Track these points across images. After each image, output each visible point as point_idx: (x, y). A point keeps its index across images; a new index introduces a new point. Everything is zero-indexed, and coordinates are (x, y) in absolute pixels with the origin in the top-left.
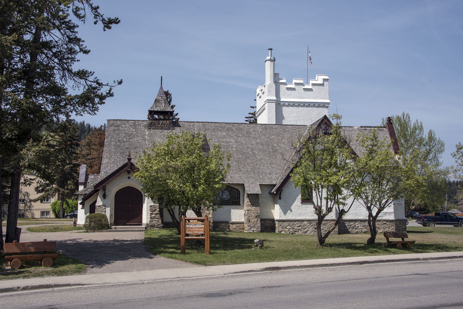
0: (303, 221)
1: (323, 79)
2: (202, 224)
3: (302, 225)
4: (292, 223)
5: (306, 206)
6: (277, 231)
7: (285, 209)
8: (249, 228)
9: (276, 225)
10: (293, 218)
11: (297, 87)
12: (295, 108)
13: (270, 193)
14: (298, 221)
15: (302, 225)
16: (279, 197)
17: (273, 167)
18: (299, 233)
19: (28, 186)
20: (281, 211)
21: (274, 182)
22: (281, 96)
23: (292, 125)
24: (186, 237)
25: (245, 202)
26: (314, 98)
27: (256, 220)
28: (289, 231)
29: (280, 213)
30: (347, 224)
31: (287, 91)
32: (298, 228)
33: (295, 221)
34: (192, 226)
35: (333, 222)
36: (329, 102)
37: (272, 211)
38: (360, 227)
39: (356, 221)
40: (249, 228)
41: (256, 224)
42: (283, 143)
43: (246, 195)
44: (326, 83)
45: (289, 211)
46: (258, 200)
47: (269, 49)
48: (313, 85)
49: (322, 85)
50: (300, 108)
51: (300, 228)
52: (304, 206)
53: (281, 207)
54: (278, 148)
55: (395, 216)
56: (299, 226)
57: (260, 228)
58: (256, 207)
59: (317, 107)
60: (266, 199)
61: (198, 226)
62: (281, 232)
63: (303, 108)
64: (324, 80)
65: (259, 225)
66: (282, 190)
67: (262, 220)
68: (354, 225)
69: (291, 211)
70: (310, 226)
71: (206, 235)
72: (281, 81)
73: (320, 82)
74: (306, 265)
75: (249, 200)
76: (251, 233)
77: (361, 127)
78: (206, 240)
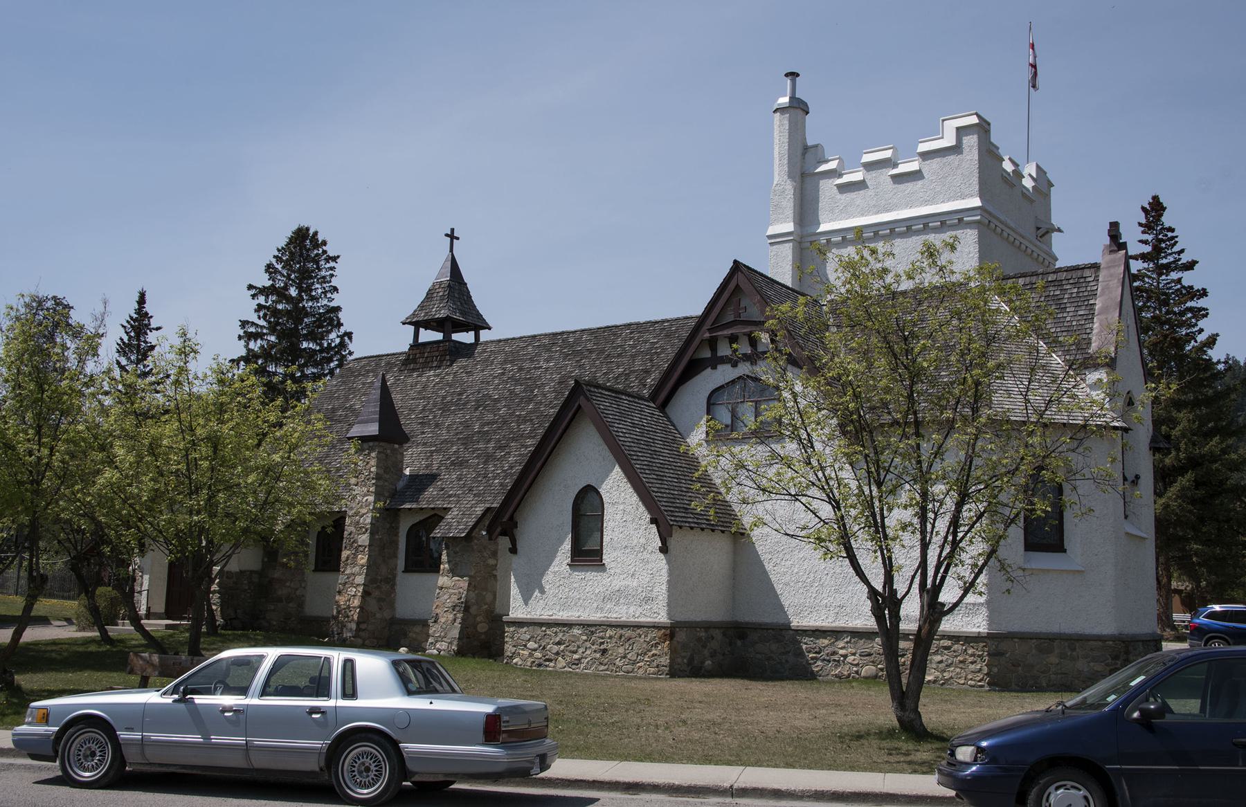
0: (568, 625)
1: (958, 129)
4: (539, 631)
5: (581, 575)
11: (871, 178)
18: (559, 665)
19: (821, 552)
22: (821, 218)
26: (926, 202)
28: (531, 655)
30: (806, 644)
31: (839, 196)
32: (555, 649)
38: (850, 659)
39: (836, 634)
45: (537, 593)
47: (787, 75)
52: (579, 575)
55: (991, 620)
56: (559, 643)
57: (455, 643)
64: (960, 131)
68: (830, 650)
69: (542, 591)
73: (949, 140)
74: (784, 788)
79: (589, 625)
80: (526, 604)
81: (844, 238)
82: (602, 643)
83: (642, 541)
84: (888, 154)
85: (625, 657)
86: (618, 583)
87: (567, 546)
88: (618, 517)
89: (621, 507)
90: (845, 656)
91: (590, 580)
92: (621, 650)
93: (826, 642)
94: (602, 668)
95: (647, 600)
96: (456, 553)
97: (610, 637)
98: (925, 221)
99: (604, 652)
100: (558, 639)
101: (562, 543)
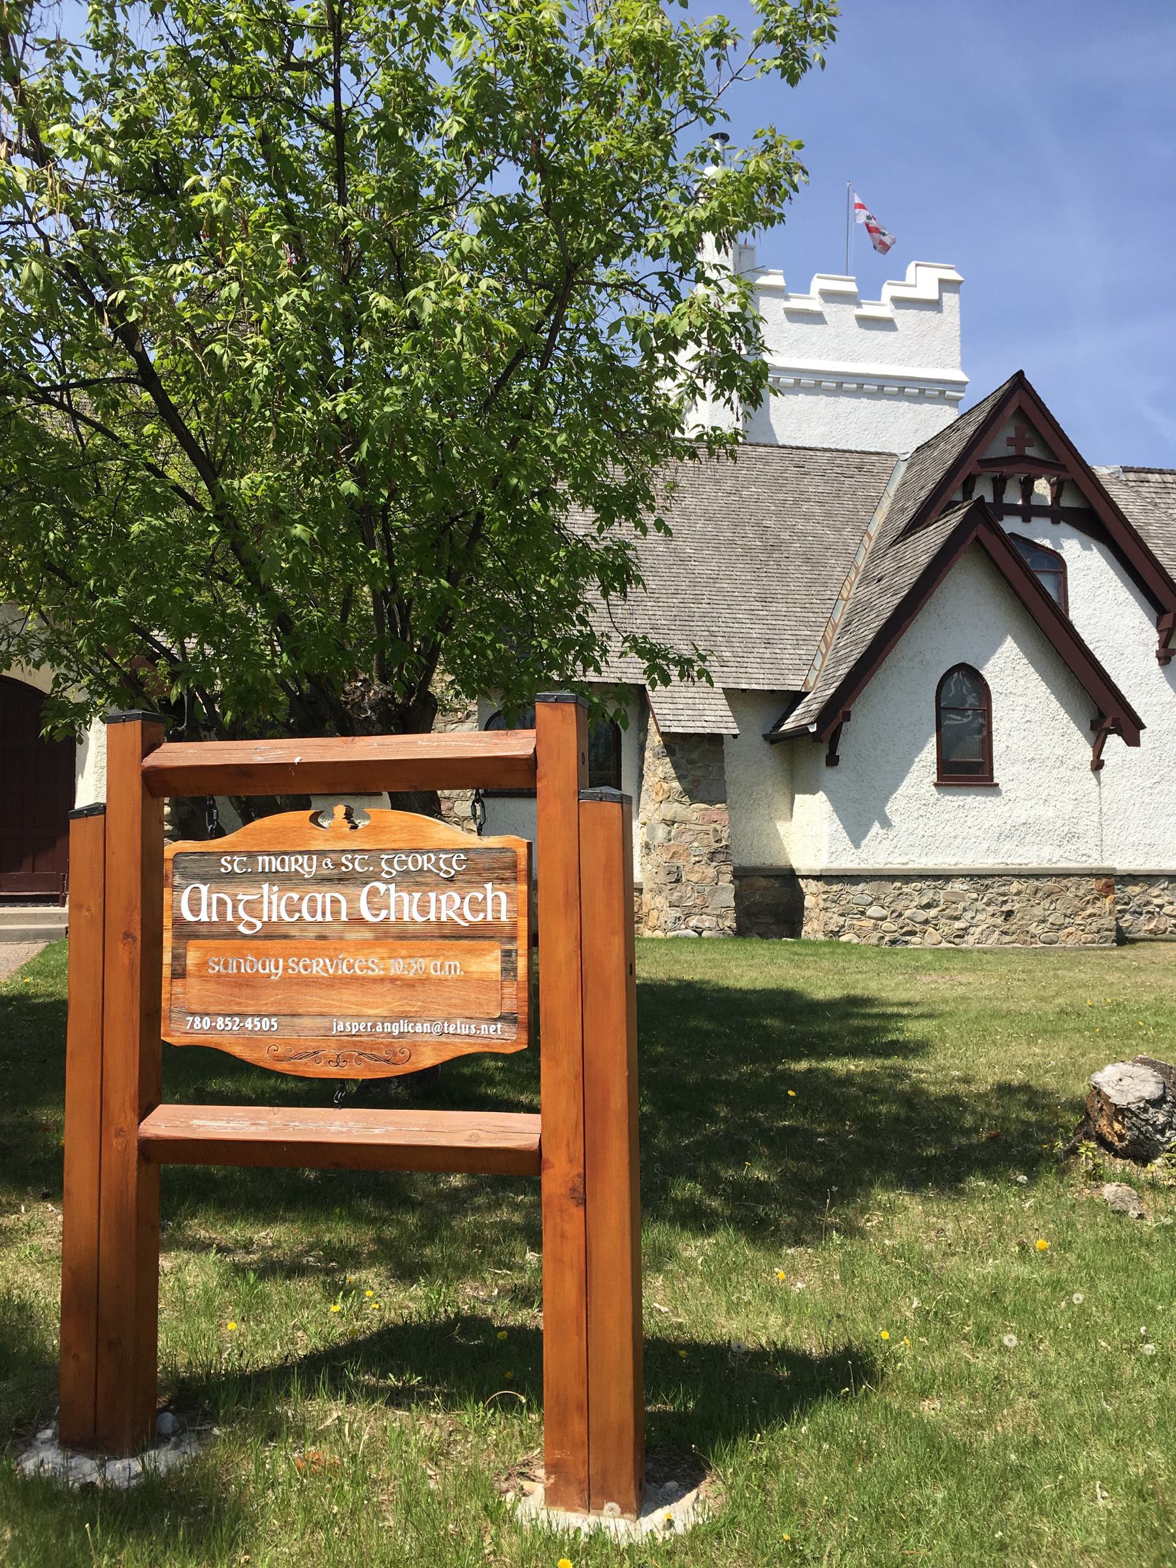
0: (944, 877)
2: (477, 869)
3: (941, 896)
4: (890, 888)
6: (811, 929)
7: (859, 817)
8: (674, 913)
9: (809, 902)
10: (895, 862)
11: (830, 311)
12: (823, 400)
13: (774, 738)
14: (922, 877)
15: (941, 896)
16: (825, 751)
17: (776, 616)
20: (838, 825)
21: (794, 683)
23: (830, 450)
24: (173, 1121)
25: (649, 780)
26: (901, 362)
27: (711, 871)
29: (833, 839)
31: (788, 325)
32: (923, 915)
33: (907, 878)
34: (273, 903)
35: (1093, 884)
36: (964, 378)
37: (782, 827)
39: (1150, 878)
40: (674, 913)
41: (713, 893)
42: (807, 517)
43: (654, 740)
44: (951, 301)
45: (876, 828)
46: (722, 770)
48: (899, 302)
49: (935, 305)
50: (844, 400)
51: (933, 912)
53: (839, 807)
54: (785, 535)
56: (928, 906)
57: (732, 914)
58: (711, 803)
59: (911, 399)
60: (750, 765)
61: (404, 906)
62: (836, 934)
63: (854, 402)
64: (945, 285)
65: (727, 896)
66: (847, 717)
67: (741, 875)
69: (886, 823)
70: (980, 905)
71: (556, 1072)
72: (763, 280)
75: (675, 766)
76: (687, 938)
77: (1126, 470)
78: (556, 1179)
79: (980, 877)
80: (857, 845)
81: (798, 382)
82: (1005, 902)
83: (1059, 751)
84: (851, 287)
85: (1044, 921)
86: (1021, 813)
87: (929, 754)
88: (1017, 715)
89: (1021, 700)
90: (1161, 907)
91: (970, 805)
92: (1038, 911)
93: (1137, 889)
94: (1007, 939)
95: (1071, 836)
96: (690, 762)
97: (1018, 893)
98: (861, 381)
99: (1009, 914)
100: (925, 901)
101: (920, 749)
